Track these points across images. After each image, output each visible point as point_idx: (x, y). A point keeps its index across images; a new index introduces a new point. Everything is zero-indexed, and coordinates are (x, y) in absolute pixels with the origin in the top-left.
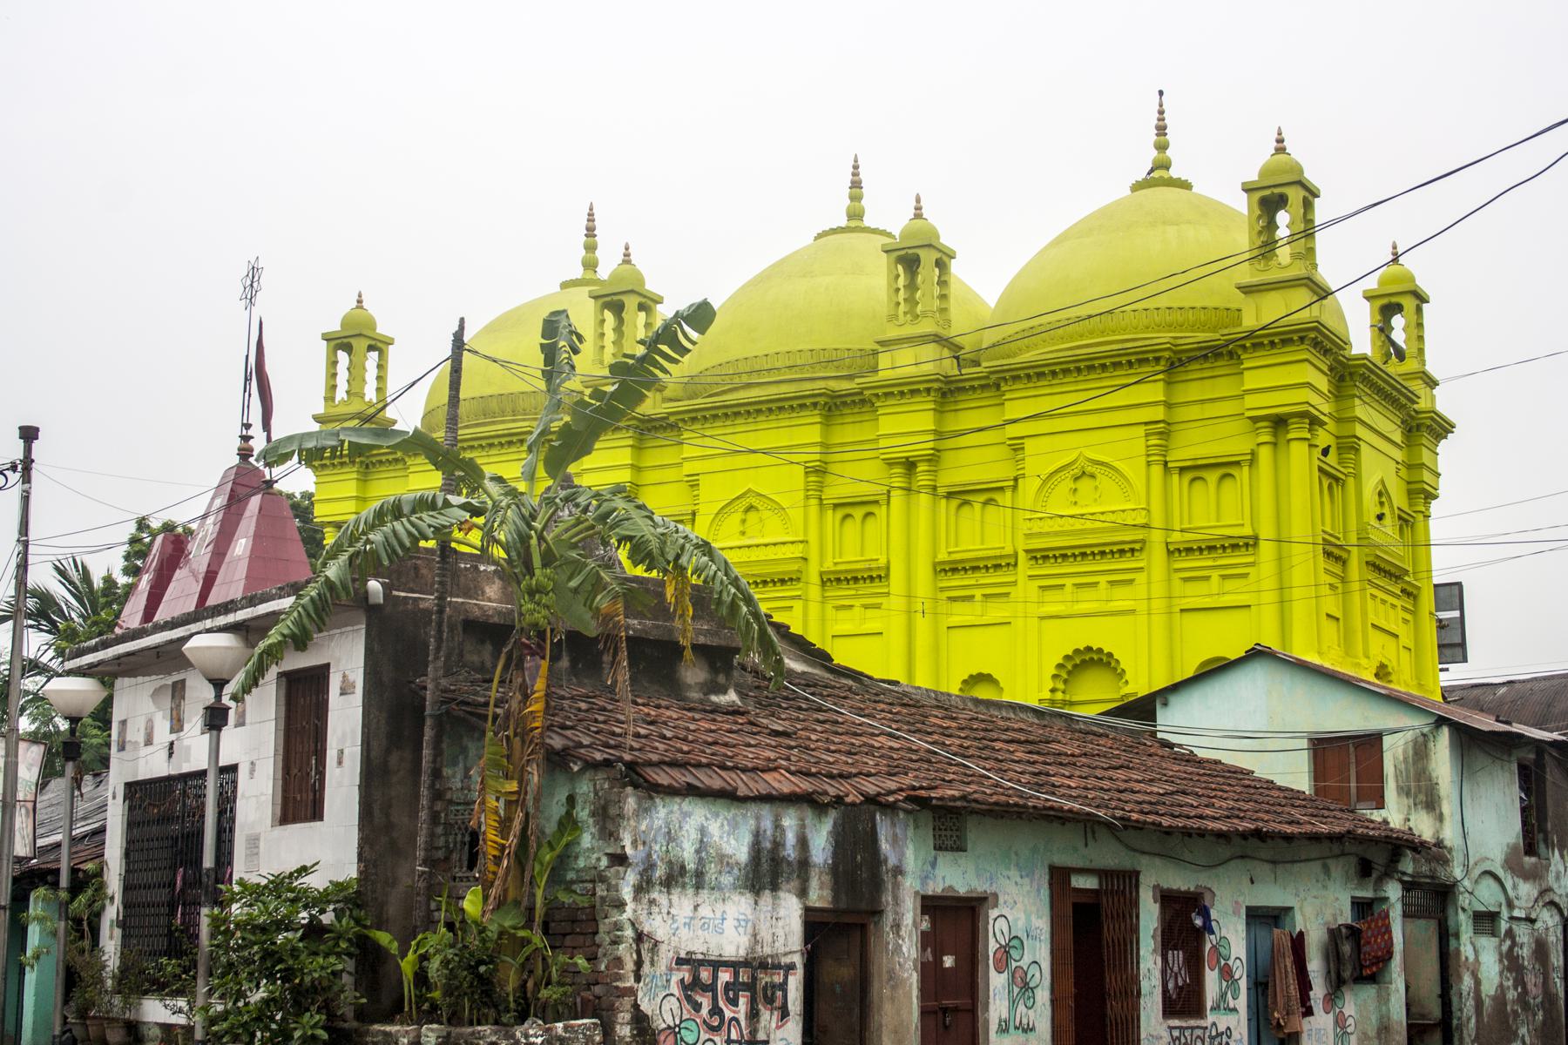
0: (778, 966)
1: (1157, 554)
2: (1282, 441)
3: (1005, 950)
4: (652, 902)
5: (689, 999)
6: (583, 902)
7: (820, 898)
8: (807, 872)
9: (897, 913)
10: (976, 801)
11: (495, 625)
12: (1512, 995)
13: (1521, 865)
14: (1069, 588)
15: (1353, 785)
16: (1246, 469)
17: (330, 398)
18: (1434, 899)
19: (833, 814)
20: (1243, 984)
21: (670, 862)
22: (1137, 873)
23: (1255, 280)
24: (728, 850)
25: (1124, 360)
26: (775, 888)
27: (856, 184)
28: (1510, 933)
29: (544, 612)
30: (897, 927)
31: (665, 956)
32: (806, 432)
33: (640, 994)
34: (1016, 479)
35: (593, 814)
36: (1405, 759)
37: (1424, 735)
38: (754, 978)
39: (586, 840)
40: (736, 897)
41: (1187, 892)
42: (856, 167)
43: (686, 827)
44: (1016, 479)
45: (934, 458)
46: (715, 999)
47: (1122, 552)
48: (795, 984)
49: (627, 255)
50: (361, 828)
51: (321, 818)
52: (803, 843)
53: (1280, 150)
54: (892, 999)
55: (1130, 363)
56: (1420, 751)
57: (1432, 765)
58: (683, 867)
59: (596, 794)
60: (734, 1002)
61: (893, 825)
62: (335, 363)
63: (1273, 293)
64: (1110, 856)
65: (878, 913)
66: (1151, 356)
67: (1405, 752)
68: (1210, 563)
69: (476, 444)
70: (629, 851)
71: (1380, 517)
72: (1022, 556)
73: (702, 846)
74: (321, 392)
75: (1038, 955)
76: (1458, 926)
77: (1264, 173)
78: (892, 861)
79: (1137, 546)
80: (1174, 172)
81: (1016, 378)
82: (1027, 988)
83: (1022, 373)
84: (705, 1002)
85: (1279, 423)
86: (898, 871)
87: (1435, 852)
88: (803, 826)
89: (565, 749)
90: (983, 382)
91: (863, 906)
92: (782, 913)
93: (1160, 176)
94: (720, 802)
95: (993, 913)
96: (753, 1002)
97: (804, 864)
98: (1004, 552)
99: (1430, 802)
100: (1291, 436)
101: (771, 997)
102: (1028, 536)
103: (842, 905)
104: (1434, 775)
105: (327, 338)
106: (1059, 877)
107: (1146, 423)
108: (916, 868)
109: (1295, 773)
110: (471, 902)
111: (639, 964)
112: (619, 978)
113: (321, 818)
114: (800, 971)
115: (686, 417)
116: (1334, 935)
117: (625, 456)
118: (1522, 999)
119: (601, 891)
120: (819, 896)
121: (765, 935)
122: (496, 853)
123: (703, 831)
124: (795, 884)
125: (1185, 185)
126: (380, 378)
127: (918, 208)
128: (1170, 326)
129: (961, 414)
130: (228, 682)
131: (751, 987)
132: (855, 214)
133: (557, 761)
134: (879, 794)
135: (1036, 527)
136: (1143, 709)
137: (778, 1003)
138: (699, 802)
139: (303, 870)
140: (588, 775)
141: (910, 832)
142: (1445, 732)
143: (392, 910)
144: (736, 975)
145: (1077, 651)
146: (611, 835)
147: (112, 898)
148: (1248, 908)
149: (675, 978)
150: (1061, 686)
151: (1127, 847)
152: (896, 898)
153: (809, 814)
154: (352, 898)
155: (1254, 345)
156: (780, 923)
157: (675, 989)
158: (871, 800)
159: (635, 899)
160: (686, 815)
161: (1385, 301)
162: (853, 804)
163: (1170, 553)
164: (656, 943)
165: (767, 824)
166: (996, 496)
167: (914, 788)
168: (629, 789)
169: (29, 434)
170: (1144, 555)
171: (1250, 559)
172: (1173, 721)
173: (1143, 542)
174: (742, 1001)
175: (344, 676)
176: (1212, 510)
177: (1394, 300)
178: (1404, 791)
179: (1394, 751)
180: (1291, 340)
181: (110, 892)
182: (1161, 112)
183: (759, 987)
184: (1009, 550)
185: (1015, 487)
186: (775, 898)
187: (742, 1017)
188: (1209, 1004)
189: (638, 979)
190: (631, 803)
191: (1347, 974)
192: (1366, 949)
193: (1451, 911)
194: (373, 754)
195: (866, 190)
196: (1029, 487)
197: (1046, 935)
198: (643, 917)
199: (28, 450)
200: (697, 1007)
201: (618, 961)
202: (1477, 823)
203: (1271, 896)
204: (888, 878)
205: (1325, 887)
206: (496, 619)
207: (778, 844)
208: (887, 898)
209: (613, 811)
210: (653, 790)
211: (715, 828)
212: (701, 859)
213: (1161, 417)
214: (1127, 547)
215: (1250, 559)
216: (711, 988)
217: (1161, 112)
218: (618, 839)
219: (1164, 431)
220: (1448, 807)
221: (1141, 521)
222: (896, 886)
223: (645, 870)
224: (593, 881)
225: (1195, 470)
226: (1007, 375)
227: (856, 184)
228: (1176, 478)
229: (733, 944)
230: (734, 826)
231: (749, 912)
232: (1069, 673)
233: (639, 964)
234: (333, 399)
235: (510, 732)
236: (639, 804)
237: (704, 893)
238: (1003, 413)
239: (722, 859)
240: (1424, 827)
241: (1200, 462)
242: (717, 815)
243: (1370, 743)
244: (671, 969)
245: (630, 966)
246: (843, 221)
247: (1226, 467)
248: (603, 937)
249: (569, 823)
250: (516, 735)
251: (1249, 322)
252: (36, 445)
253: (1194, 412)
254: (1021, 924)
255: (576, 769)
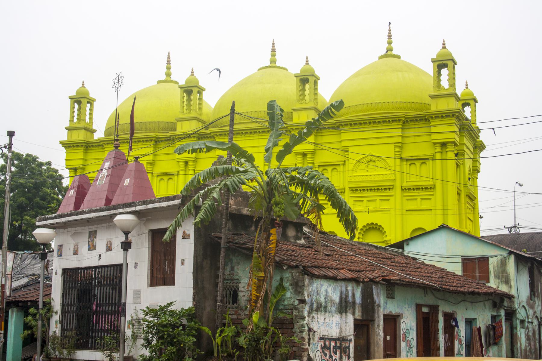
0: (347, 340)
1: (398, 190)
2: (187, 170)
3: (405, 334)
4: (313, 317)
5: (323, 352)
6: (288, 317)
7: (358, 315)
8: (355, 306)
9: (378, 321)
10: (403, 281)
11: (234, 214)
12: (528, 349)
13: (530, 303)
14: (365, 201)
15: (477, 274)
16: (176, 177)
17: (71, 121)
18: (511, 314)
19: (361, 285)
20: (464, 345)
21: (318, 303)
22: (438, 306)
23: (436, 93)
24: (333, 298)
25: (387, 120)
26: (346, 312)
27: (273, 50)
28: (528, 327)
29: (283, 211)
30: (379, 325)
31: (317, 337)
32: (396, 131)
33: (310, 350)
34: (345, 161)
35: (291, 285)
36: (497, 266)
37: (505, 258)
38: (341, 344)
39: (288, 294)
40: (336, 315)
41: (450, 313)
42: (273, 44)
43: (322, 290)
44: (345, 161)
45: (313, 153)
46: (330, 352)
47: (385, 189)
48: (352, 346)
49: (192, 72)
50: (194, 288)
51: (173, 283)
52: (353, 295)
53: (444, 47)
54: (378, 352)
55: (389, 121)
56: (503, 263)
57: (508, 268)
58: (321, 304)
59: (293, 277)
60: (335, 353)
61: (377, 289)
62: (74, 107)
63: (442, 99)
64: (430, 300)
65: (373, 321)
66: (397, 119)
67: (497, 263)
68: (417, 194)
69: (125, 141)
70: (306, 298)
71: (469, 179)
72: (347, 190)
73: (326, 297)
74: (68, 119)
75: (413, 335)
76: (517, 325)
77: (438, 55)
78: (377, 302)
79: (391, 187)
80: (394, 52)
81: (346, 125)
82: (410, 347)
83: (349, 123)
84: (328, 353)
85: (444, 145)
86: (379, 306)
87: (510, 297)
88: (353, 290)
89: (280, 261)
90: (333, 126)
91: (370, 318)
92: (348, 321)
93: (389, 54)
94: (331, 281)
95: (402, 321)
96: (341, 353)
97: (354, 303)
98: (340, 188)
99: (507, 282)
100: (448, 150)
101: (344, 351)
102: (350, 182)
103: (364, 318)
104: (508, 272)
105: (71, 98)
106: (418, 307)
107: (394, 143)
108: (385, 306)
109: (457, 269)
110: (255, 317)
111: (309, 339)
112: (304, 345)
113: (173, 283)
114: (353, 342)
115: (218, 134)
116: (488, 327)
117: (150, 150)
118: (530, 351)
119: (295, 313)
120: (358, 315)
121: (344, 329)
122: (255, 299)
123: (326, 291)
124: (351, 310)
125: (399, 57)
126: (91, 114)
127: (307, 61)
128: (404, 109)
129: (323, 137)
130: (130, 232)
131: (340, 348)
132: (273, 61)
133: (279, 265)
134: (374, 278)
135: (353, 179)
136: (400, 245)
137: (347, 354)
138: (325, 281)
139: (170, 304)
140: (289, 270)
141: (382, 292)
142: (512, 257)
143: (205, 318)
144: (336, 343)
145: (368, 224)
146: (300, 292)
147: (56, 313)
148: (466, 319)
149: (319, 345)
150: (361, 237)
151: (436, 297)
152: (378, 315)
153: (355, 285)
154: (191, 315)
155: (435, 117)
156: (348, 325)
157: (319, 349)
158: (372, 281)
159: (308, 316)
160: (322, 285)
161: (464, 102)
162: (367, 282)
163: (402, 190)
164: (315, 332)
165: (344, 289)
166: (337, 167)
167: (383, 276)
168: (306, 276)
169: (11, 134)
170: (393, 191)
171: (432, 193)
172: (411, 250)
173: (393, 185)
174: (338, 353)
175: (184, 232)
176: (418, 175)
177: (467, 101)
178: (497, 277)
179: (493, 263)
180: (449, 116)
181: (55, 310)
182: (390, 31)
183: (343, 347)
184: (342, 187)
185: (344, 164)
186: (346, 315)
187: (338, 358)
188: (456, 353)
189: (309, 345)
190: (307, 281)
191: (492, 342)
192: (496, 333)
193: (514, 320)
194: (198, 261)
195: (277, 53)
196: (350, 165)
197: (415, 329)
198: (310, 323)
199: (11, 140)
200: (326, 355)
201: (303, 338)
202: (519, 287)
203: (471, 315)
204: (376, 308)
205: (484, 311)
206: (234, 212)
207: (347, 296)
208: (376, 315)
209: (300, 284)
210: (313, 276)
211: (330, 290)
212: (326, 301)
213: (400, 141)
214: (387, 187)
215: (432, 193)
216: (329, 348)
217: (390, 31)
218: (303, 294)
219: (401, 146)
220: (513, 283)
221: (393, 178)
222: (378, 311)
223: (311, 305)
224: (292, 309)
225: (411, 160)
226: (343, 124)
227: (273, 50)
228: (405, 163)
229: (334, 333)
230: (335, 290)
231: (339, 320)
232: (364, 232)
233: (309, 339)
234: (73, 121)
235: (261, 254)
236: (309, 281)
237: (327, 313)
238: (341, 138)
239: (332, 301)
240: (504, 288)
241: (414, 158)
242: (330, 286)
243: (484, 260)
244: (318, 341)
245: (307, 340)
246: (268, 64)
247: (424, 160)
248: (296, 329)
249: (281, 287)
250: (263, 255)
251: (433, 108)
252: (13, 138)
253: (412, 140)
254: (409, 325)
255: (285, 268)
